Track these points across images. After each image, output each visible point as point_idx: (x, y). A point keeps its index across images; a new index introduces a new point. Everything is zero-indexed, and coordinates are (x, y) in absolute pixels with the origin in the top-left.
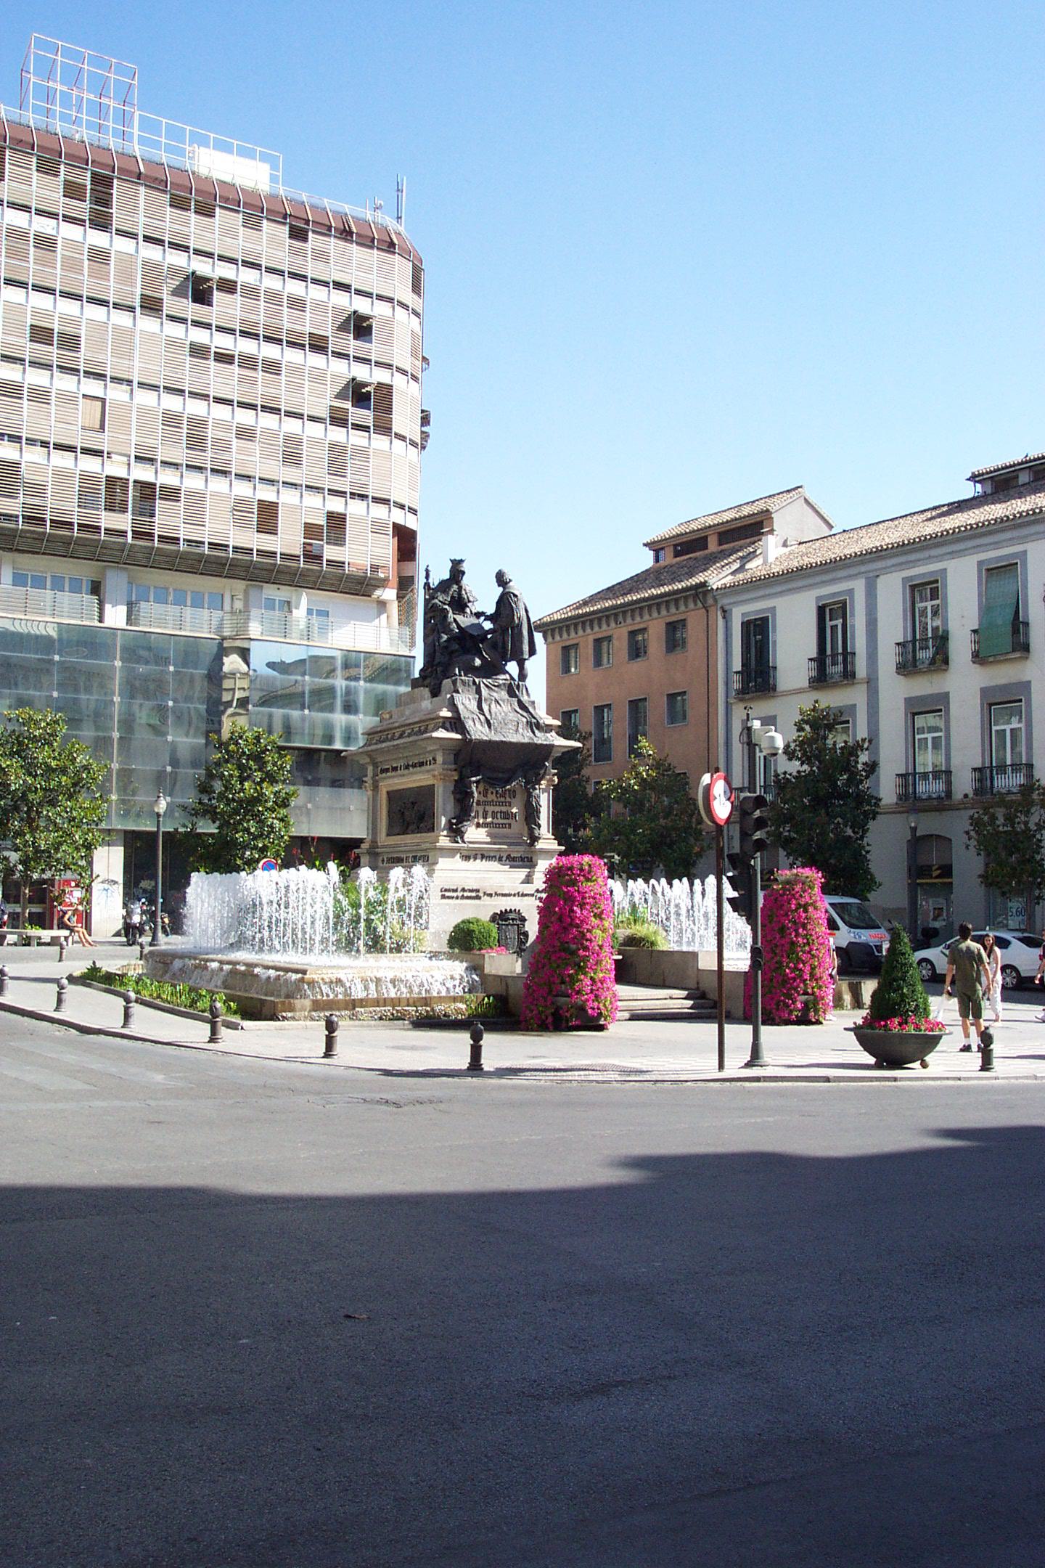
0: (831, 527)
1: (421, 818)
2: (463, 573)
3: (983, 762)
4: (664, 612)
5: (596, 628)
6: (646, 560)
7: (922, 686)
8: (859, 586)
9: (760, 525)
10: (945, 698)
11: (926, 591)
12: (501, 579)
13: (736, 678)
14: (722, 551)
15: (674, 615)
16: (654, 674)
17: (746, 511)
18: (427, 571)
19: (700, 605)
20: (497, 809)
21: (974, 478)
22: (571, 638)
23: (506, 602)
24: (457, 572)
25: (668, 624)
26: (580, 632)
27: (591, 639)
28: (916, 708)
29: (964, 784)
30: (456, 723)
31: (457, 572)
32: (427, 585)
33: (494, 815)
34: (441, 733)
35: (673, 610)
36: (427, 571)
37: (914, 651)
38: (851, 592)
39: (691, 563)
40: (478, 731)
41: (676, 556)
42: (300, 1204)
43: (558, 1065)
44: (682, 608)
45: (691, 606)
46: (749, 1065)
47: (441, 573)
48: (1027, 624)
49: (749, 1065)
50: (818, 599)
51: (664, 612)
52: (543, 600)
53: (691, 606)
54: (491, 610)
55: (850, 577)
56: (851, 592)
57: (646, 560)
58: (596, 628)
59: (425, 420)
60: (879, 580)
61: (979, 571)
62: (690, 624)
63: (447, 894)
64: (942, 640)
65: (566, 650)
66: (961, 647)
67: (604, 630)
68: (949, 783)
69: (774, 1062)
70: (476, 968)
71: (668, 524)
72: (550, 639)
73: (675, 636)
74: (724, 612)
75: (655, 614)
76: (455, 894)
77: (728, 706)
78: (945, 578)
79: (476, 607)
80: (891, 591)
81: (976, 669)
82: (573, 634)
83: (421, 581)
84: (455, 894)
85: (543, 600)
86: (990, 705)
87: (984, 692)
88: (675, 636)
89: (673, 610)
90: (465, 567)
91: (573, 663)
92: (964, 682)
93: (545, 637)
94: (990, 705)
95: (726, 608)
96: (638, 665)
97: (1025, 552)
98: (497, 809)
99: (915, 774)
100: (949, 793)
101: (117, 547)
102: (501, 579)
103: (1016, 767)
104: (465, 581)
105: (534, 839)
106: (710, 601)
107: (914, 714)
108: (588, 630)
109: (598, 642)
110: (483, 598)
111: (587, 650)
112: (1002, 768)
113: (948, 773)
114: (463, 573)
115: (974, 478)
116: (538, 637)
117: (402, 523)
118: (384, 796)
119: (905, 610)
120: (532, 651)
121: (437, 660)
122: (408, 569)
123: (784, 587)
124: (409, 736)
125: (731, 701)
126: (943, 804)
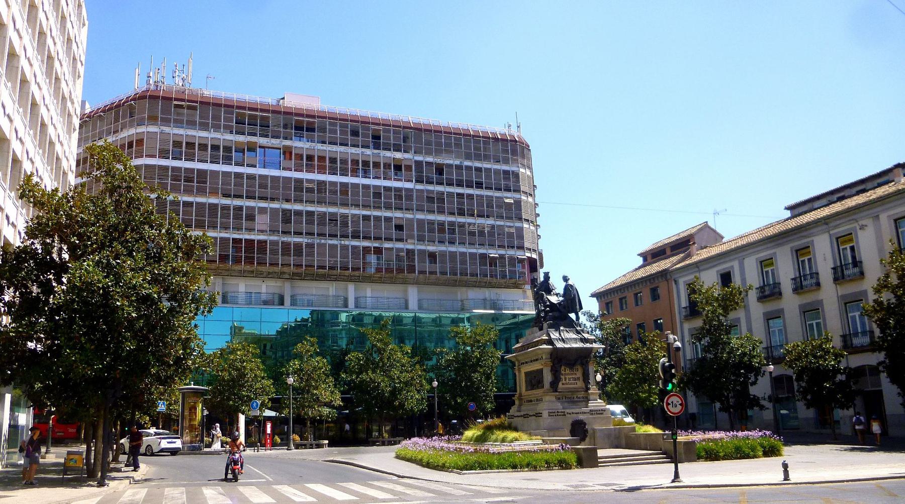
7: (772, 306)
8: (736, 264)
9: (689, 241)
11: (802, 252)
12: (565, 279)
16: (646, 310)
17: (682, 235)
22: (609, 298)
28: (769, 317)
30: (550, 342)
33: (569, 379)
34: (545, 346)
37: (842, 271)
38: (732, 267)
40: (560, 345)
46: (673, 481)
48: (861, 262)
49: (673, 481)
55: (731, 261)
56: (732, 267)
57: (640, 261)
65: (607, 304)
69: (685, 480)
70: (834, 431)
71: (648, 245)
73: (655, 295)
78: (813, 245)
79: (557, 291)
80: (751, 264)
81: (796, 296)
86: (804, 312)
87: (800, 306)
88: (655, 295)
92: (790, 302)
94: (846, 304)
97: (775, 253)
102: (565, 279)
103: (864, 333)
105: (588, 389)
106: (669, 277)
107: (768, 320)
109: (621, 299)
111: (617, 302)
112: (856, 334)
118: (523, 375)
123: (785, 240)
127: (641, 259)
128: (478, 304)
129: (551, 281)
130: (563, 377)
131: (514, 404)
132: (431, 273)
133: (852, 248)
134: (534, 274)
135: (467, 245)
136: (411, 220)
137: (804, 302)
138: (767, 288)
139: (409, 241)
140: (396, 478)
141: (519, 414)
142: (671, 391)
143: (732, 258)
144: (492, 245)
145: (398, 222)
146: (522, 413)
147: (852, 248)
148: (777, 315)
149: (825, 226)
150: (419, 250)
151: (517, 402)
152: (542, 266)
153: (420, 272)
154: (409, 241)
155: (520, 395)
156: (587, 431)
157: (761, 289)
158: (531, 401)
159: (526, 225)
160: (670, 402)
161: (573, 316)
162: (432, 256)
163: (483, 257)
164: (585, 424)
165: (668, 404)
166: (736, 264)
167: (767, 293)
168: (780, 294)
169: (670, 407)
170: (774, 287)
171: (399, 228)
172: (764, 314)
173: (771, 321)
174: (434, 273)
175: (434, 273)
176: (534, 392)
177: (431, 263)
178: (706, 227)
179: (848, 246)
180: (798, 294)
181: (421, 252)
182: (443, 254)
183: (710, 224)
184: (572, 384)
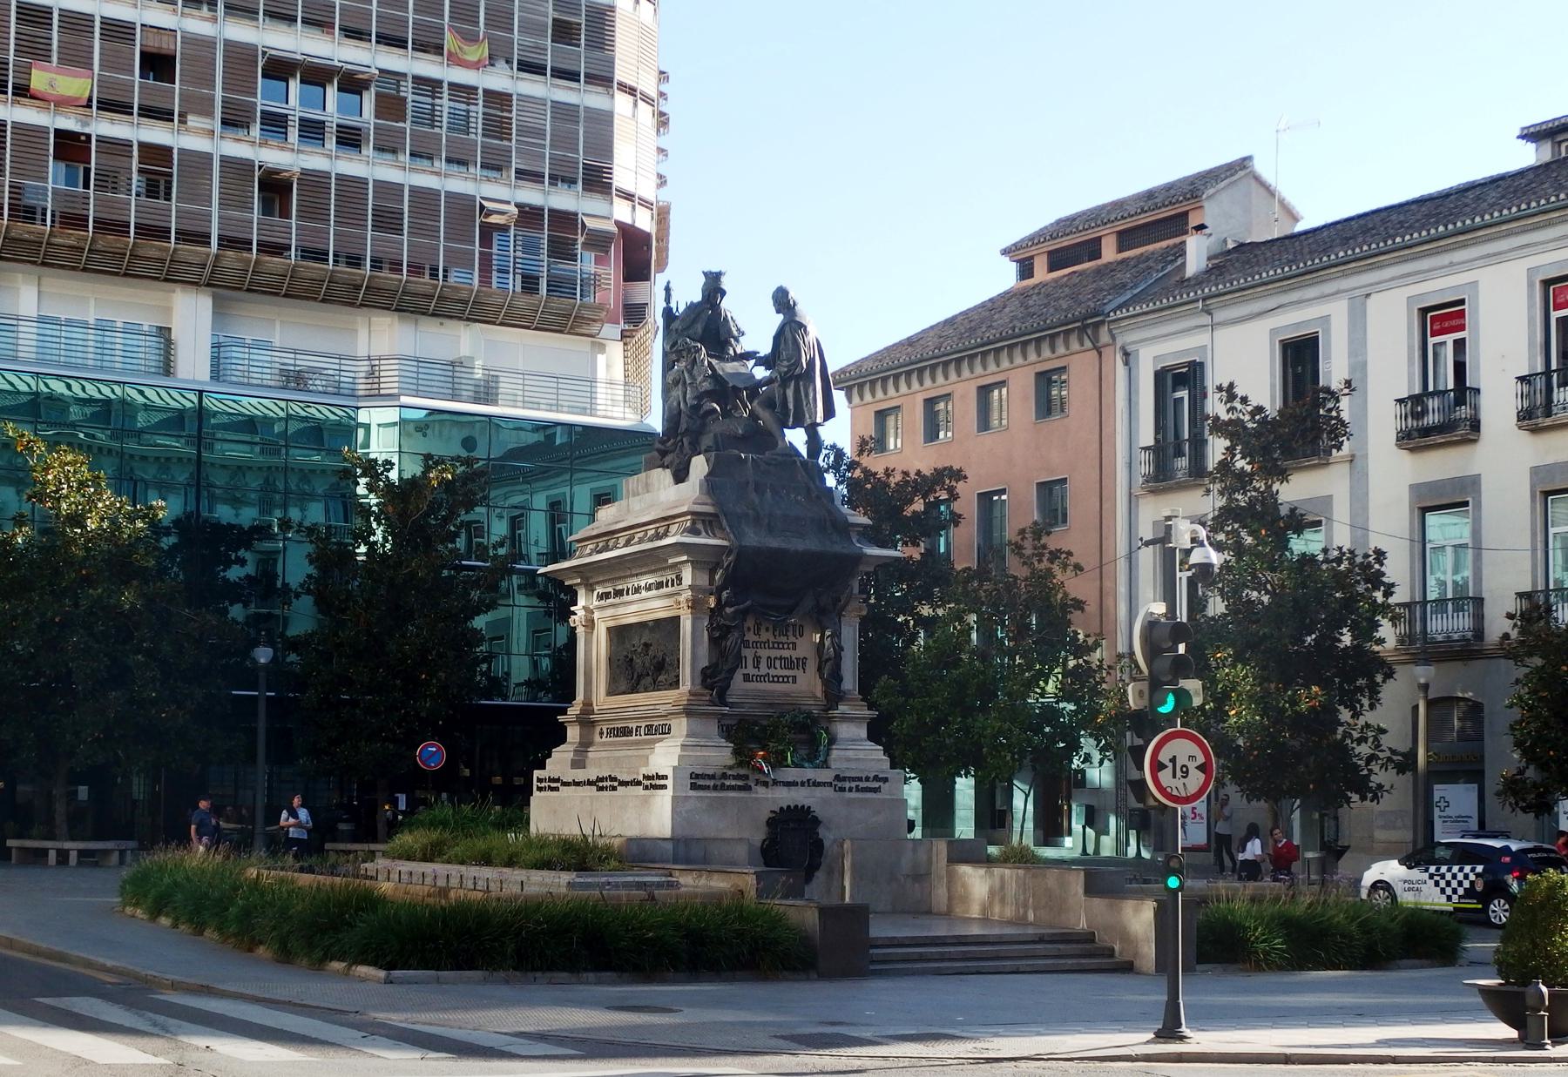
0: (1296, 219)
1: (660, 667)
2: (723, 293)
3: (1534, 583)
4: (1032, 357)
5: (928, 382)
6: (1006, 277)
7: (1441, 465)
8: (1338, 311)
10: (1473, 483)
12: (782, 301)
13: (1144, 456)
14: (1123, 261)
15: (1047, 358)
18: (668, 289)
19: (1088, 344)
20: (774, 653)
21: (1533, 135)
23: (790, 330)
24: (713, 287)
25: (1038, 374)
26: (903, 388)
27: (920, 398)
29: (1498, 625)
31: (713, 287)
32: (668, 314)
33: (771, 663)
35: (1046, 353)
36: (668, 289)
38: (1326, 319)
39: (1076, 280)
41: (1051, 270)
42: (1470, 195)
43: (1091, 1064)
44: (1061, 350)
45: (1075, 346)
47: (688, 293)
48: (1478, 391)
50: (1274, 332)
51: (1032, 357)
52: (844, 337)
53: (1075, 346)
54: (765, 348)
56: (1326, 319)
57: (1006, 277)
58: (928, 382)
59: (663, 76)
60: (1371, 302)
61: (1531, 285)
62: (1073, 370)
63: (701, 782)
64: (1464, 391)
65: (881, 416)
66: (1498, 402)
67: (936, 385)
68: (1479, 617)
72: (856, 399)
74: (1126, 354)
75: (1019, 360)
76: (862, 785)
77: (1131, 498)
79: (745, 345)
82: (891, 391)
83: (658, 305)
84: (711, 783)
85: (844, 337)
86: (1547, 494)
89: (1046, 353)
90: (726, 283)
91: (892, 432)
93: (849, 398)
95: (1129, 349)
96: (987, 439)
98: (774, 653)
99: (1424, 602)
100: (1479, 633)
101: (197, 260)
102: (782, 301)
104: (726, 304)
106: (1104, 337)
107: (1424, 510)
108: (916, 385)
110: (756, 330)
113: (1479, 601)
114: (723, 293)
115: (1533, 135)
116: (839, 397)
117: (629, 221)
119: (1410, 348)
120: (829, 413)
121: (683, 426)
122: (639, 291)
124: (641, 541)
125: (1137, 491)
126: (1467, 650)
127: (1012, 268)
128: (393, 387)
129: (727, 305)
130: (748, 653)
131: (561, 739)
132: (265, 247)
133: (1460, 345)
134: (640, 286)
135: (405, 158)
136: (208, 44)
137: (1550, 460)
138: (1433, 403)
139: (193, 120)
140: (1097, 1064)
141: (580, 775)
142: (1169, 719)
143: (1329, 288)
144: (494, 165)
145: (155, 44)
146: (592, 773)
147: (1460, 345)
148: (1454, 498)
149: (1206, 319)
150: (226, 161)
151: (573, 733)
152: (662, 266)
153: (227, 242)
154: (193, 120)
155: (588, 707)
156: (819, 844)
157: (1414, 404)
158: (626, 732)
159: (622, 102)
160: (1164, 757)
161: (796, 437)
162: (275, 187)
163: (463, 207)
164: (816, 821)
165: (1157, 766)
166: (1338, 311)
167: (1432, 419)
168: (1475, 425)
169: (1165, 777)
170: (1460, 401)
171: (158, 64)
172: (1415, 488)
173: (1432, 519)
174: (280, 249)
175: (280, 249)
176: (641, 699)
177: (267, 209)
178: (1240, 167)
179: (1449, 339)
180: (1536, 430)
181: (236, 169)
182: (314, 182)
183: (1261, 167)
184: (776, 679)
